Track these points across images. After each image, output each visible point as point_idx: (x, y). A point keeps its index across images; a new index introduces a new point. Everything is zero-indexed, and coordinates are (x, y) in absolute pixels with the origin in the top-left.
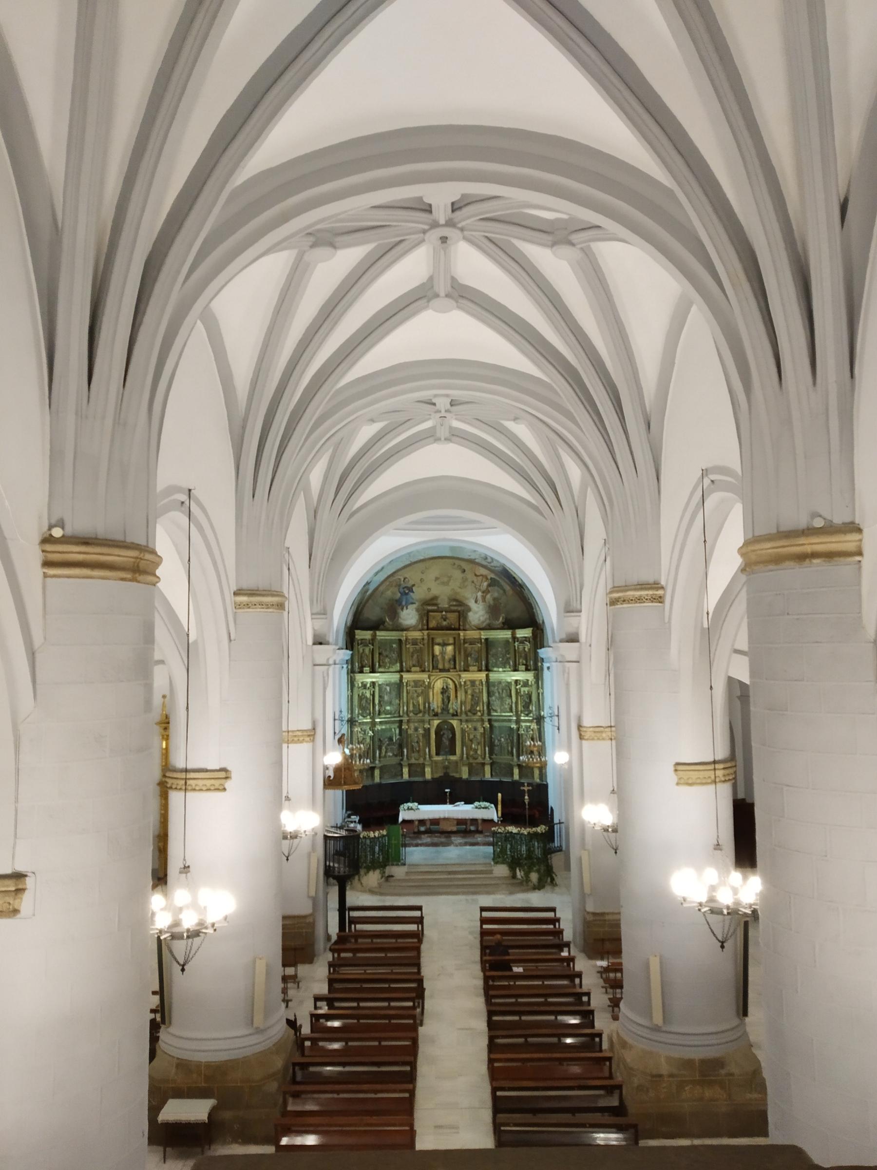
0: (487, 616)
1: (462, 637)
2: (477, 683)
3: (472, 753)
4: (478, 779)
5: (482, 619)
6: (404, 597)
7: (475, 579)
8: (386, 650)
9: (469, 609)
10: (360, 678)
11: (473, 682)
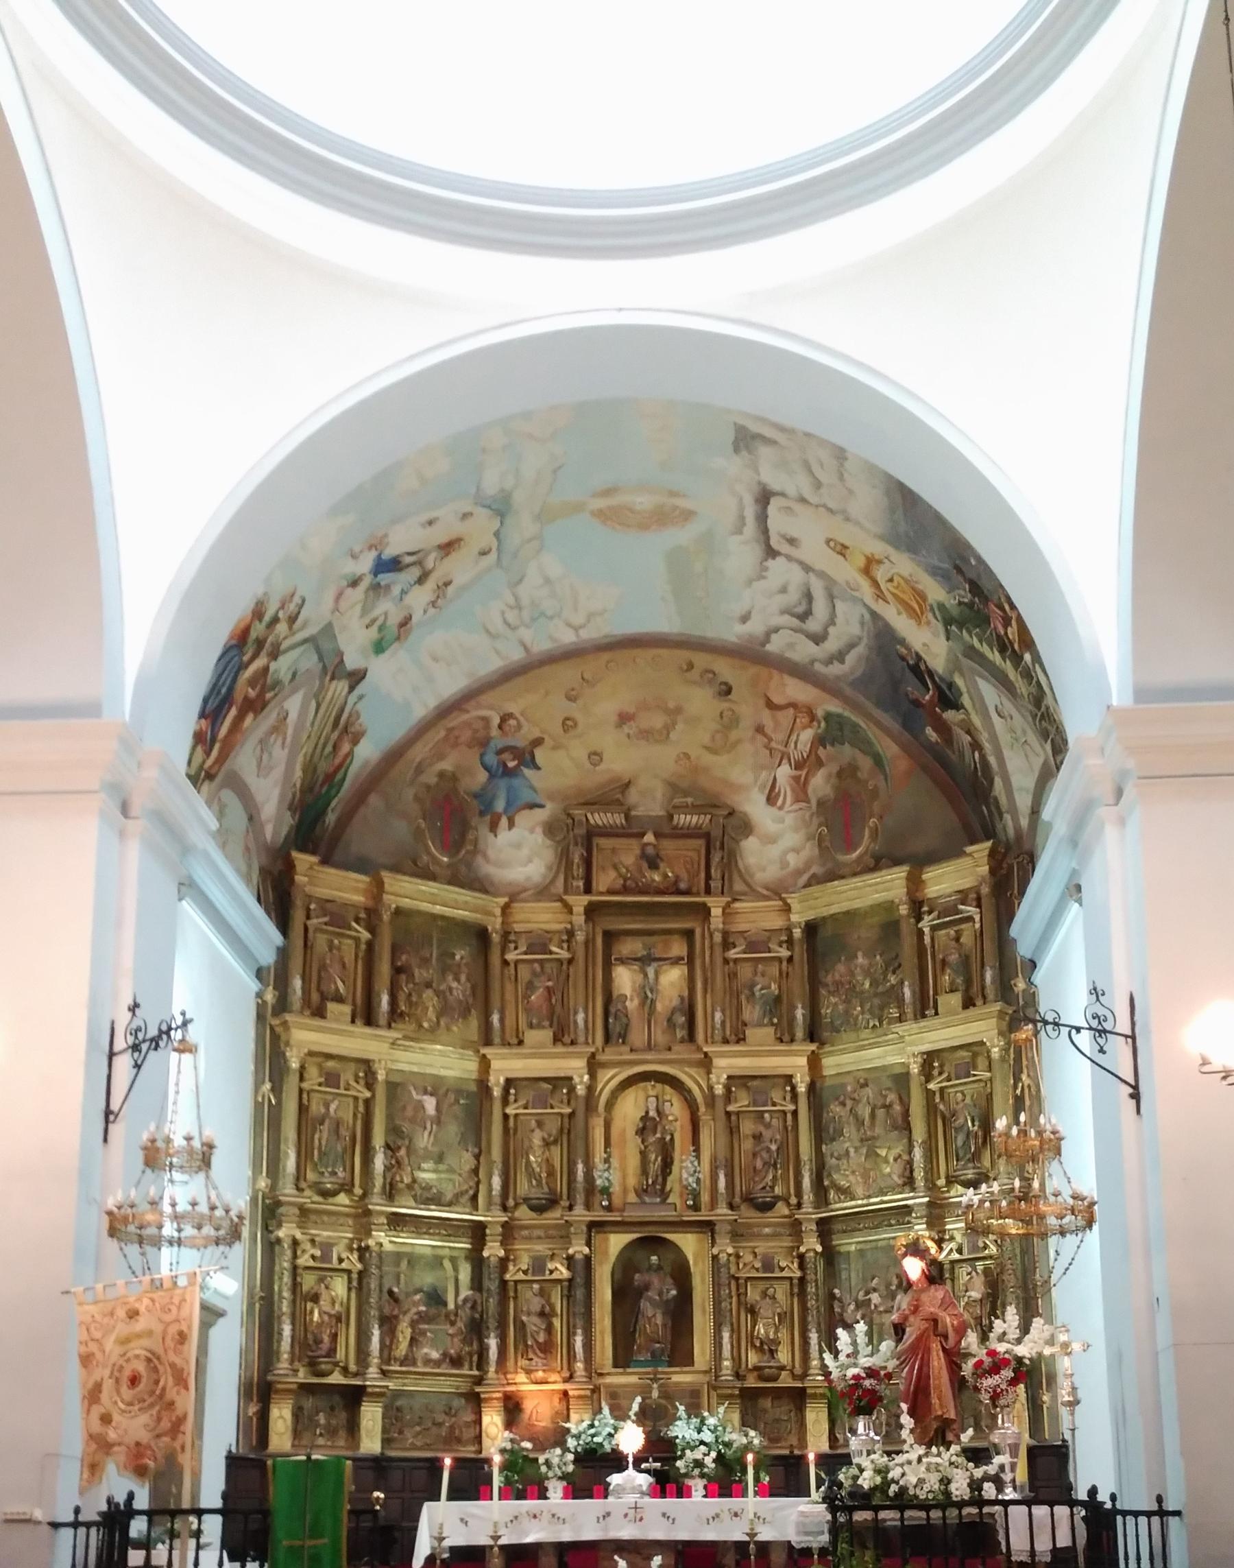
0: (810, 850)
3: (753, 1358)
5: (793, 861)
6: (502, 784)
7: (766, 717)
8: (425, 962)
10: (305, 1036)
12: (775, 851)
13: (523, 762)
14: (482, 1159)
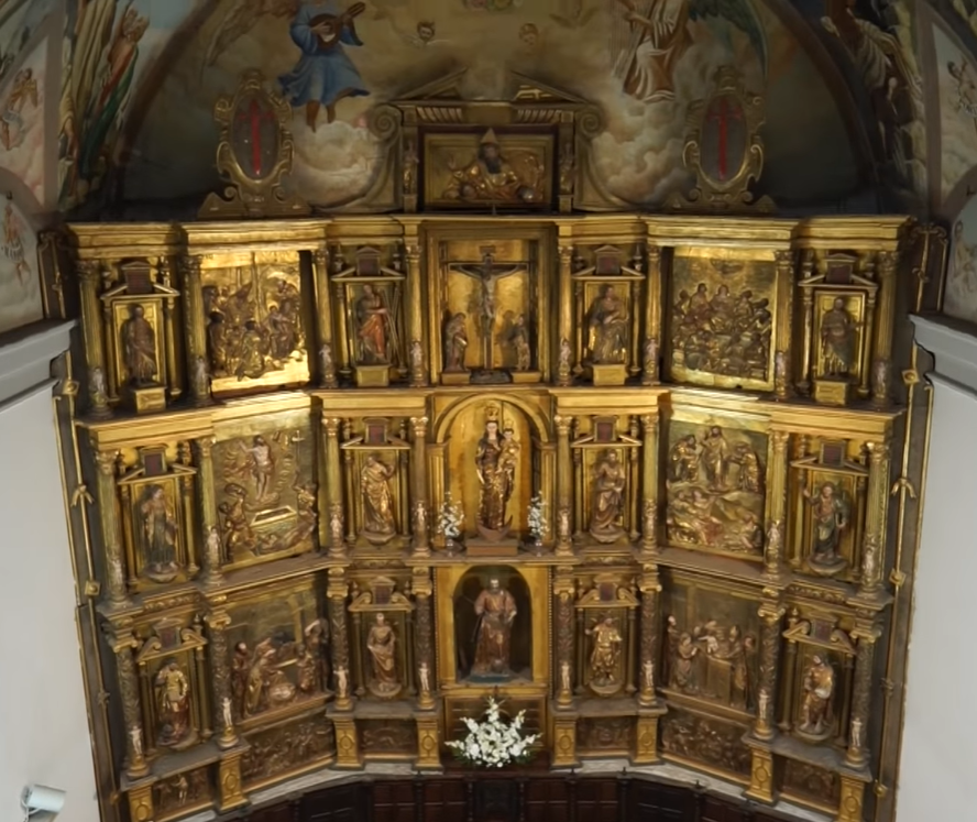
1: (565, 244)
2: (621, 425)
4: (613, 766)
5: (652, 162)
6: (319, 62)
9: (599, 120)
10: (119, 437)
11: (604, 428)
12: (631, 149)
13: (339, 37)
14: (320, 493)
